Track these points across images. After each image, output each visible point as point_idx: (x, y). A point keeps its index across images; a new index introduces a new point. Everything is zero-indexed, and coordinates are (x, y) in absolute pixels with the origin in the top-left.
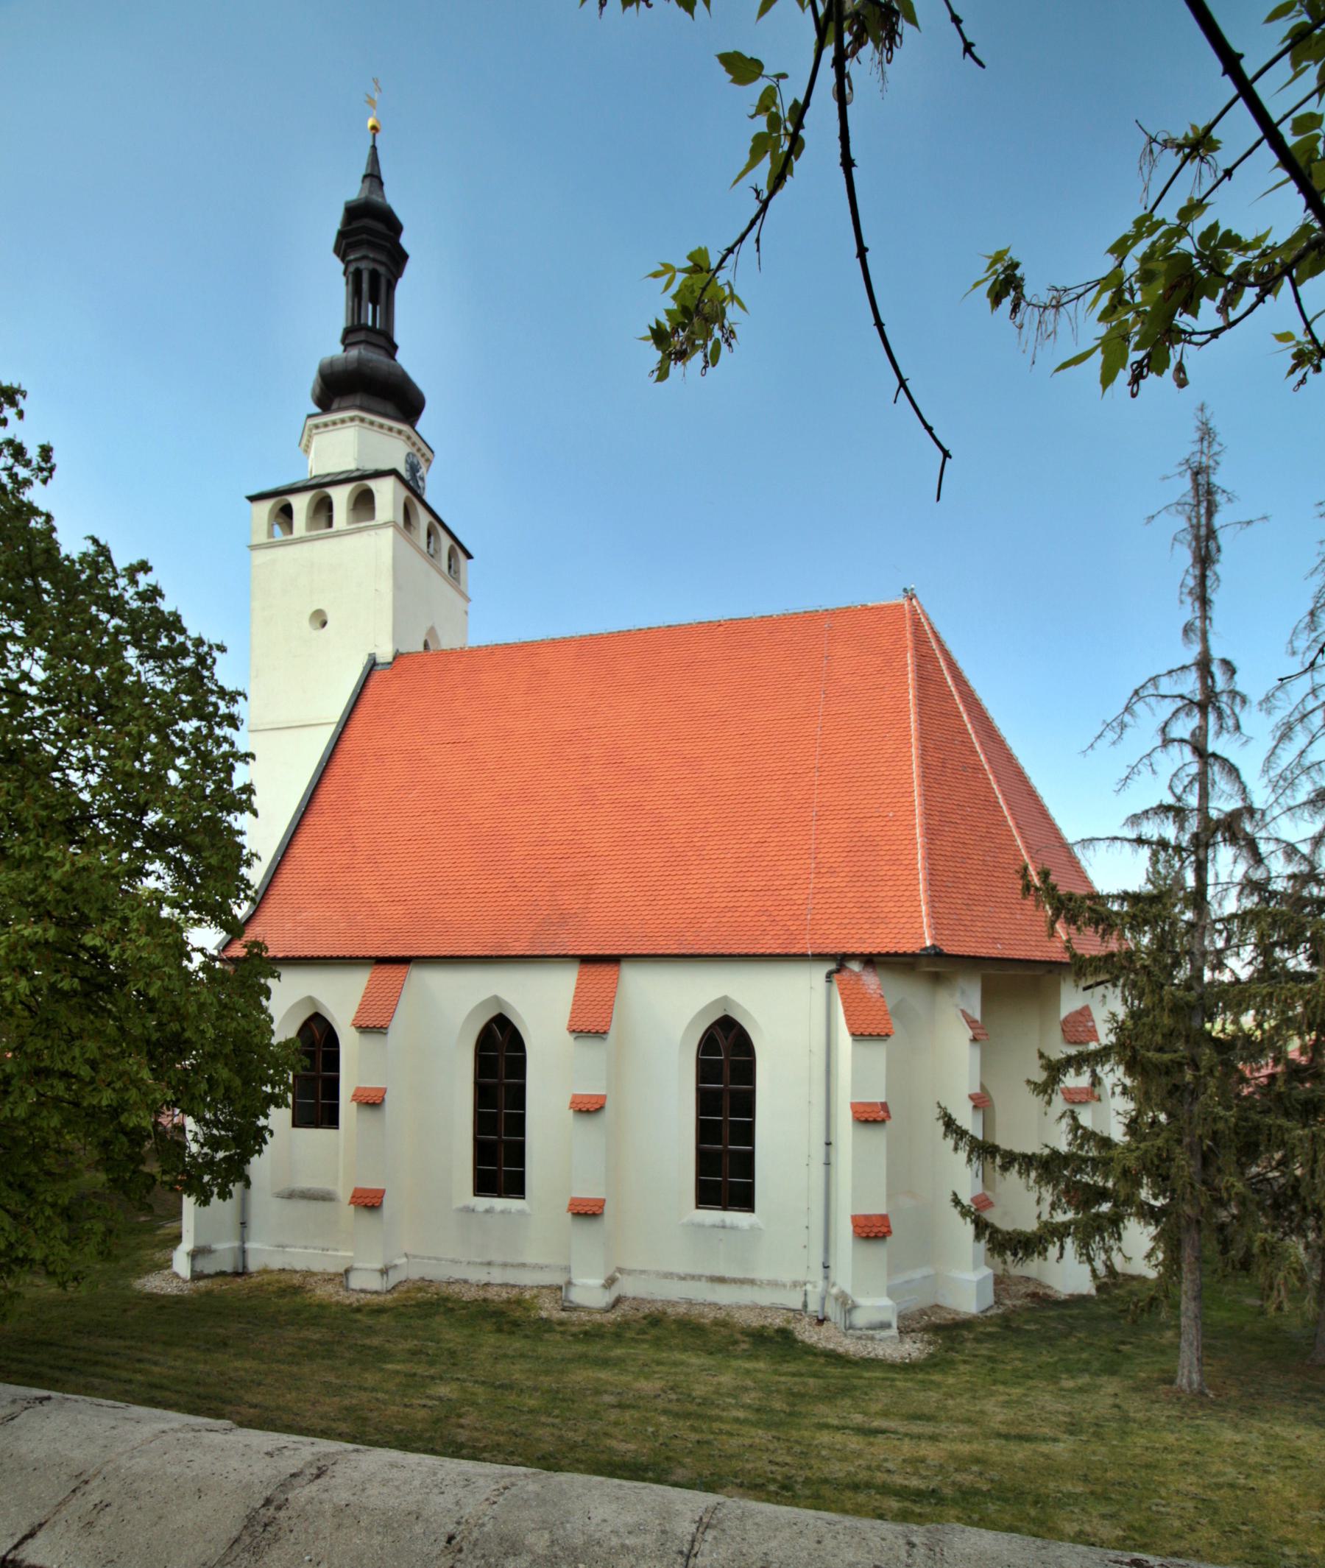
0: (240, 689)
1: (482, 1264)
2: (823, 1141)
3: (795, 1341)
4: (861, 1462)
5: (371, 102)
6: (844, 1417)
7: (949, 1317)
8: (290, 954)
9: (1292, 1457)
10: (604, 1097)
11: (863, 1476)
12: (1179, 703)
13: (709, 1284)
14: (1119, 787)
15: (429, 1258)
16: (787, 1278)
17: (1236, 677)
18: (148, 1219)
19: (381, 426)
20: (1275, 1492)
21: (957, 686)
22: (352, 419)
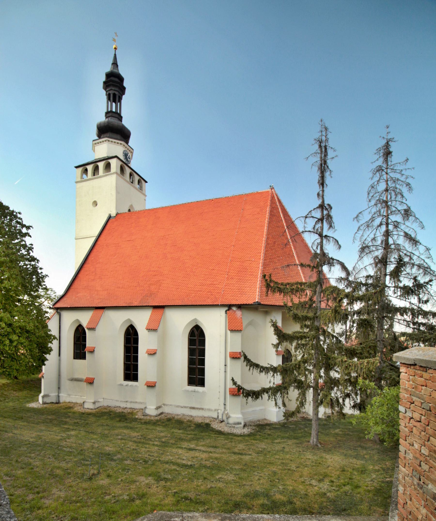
0: (31, 225)
1: (125, 402)
2: (224, 364)
5: (114, 40)
7: (266, 422)
8: (71, 306)
10: (157, 350)
13: (190, 409)
15: (110, 400)
16: (213, 408)
18: (8, 381)
19: (115, 142)
22: (106, 141)
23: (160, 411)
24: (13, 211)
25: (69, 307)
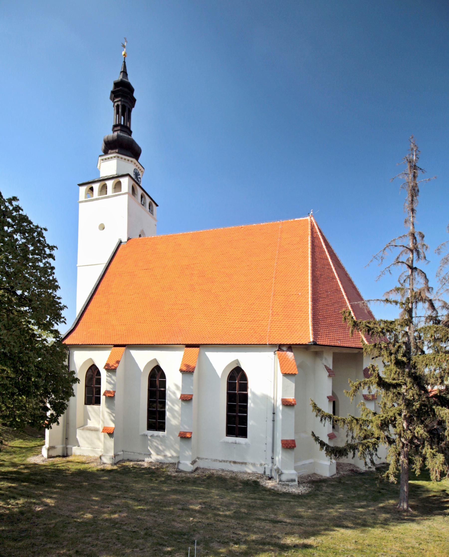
0: (55, 245)
2: (272, 412)
3: (260, 485)
4: (269, 534)
6: (267, 516)
7: (319, 478)
9: (439, 537)
11: (268, 540)
12: (402, 249)
14: (377, 279)
15: (131, 452)
17: (424, 239)
20: (430, 551)
21: (327, 248)
22: (115, 157)
23: (196, 466)
24: (37, 227)
25: (80, 343)
